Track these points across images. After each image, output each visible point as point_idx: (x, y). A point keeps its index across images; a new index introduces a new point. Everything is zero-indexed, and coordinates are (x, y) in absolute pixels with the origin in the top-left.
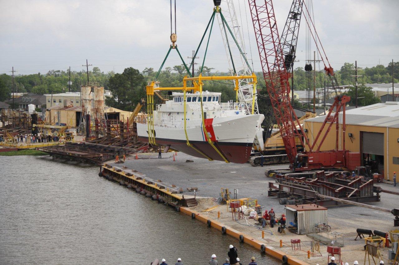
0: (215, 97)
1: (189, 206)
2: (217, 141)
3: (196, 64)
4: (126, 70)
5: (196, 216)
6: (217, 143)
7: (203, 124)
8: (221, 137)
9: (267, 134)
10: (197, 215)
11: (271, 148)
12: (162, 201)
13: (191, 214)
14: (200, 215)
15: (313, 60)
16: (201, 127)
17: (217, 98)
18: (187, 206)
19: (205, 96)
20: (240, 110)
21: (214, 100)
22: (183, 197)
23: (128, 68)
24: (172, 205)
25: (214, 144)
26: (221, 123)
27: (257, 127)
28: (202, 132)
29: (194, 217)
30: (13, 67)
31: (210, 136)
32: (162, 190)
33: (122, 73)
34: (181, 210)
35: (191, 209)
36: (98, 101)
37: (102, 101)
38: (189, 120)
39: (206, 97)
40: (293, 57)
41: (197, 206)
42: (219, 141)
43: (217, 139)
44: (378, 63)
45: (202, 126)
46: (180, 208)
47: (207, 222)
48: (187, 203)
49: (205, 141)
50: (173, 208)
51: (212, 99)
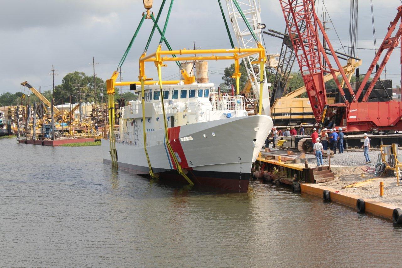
1: (317, 180)
3: (327, 29)
5: (332, 196)
6: (191, 173)
7: (166, 139)
8: (196, 162)
9: (277, 91)
10: (334, 193)
11: (281, 114)
12: (269, 178)
13: (322, 194)
14: (342, 193)
16: (164, 143)
18: (314, 182)
19: (184, 89)
20: (233, 111)
21: (200, 95)
22: (306, 165)
24: (287, 183)
25: (186, 175)
28: (167, 153)
30: (40, 87)
31: (179, 160)
34: (303, 189)
35: (321, 185)
36: (200, 79)
37: (206, 79)
38: (154, 130)
39: (186, 91)
41: (335, 181)
42: (194, 169)
45: (166, 141)
46: (300, 185)
47: (355, 204)
48: (314, 176)
49: (173, 168)
50: (289, 187)
51: (197, 94)
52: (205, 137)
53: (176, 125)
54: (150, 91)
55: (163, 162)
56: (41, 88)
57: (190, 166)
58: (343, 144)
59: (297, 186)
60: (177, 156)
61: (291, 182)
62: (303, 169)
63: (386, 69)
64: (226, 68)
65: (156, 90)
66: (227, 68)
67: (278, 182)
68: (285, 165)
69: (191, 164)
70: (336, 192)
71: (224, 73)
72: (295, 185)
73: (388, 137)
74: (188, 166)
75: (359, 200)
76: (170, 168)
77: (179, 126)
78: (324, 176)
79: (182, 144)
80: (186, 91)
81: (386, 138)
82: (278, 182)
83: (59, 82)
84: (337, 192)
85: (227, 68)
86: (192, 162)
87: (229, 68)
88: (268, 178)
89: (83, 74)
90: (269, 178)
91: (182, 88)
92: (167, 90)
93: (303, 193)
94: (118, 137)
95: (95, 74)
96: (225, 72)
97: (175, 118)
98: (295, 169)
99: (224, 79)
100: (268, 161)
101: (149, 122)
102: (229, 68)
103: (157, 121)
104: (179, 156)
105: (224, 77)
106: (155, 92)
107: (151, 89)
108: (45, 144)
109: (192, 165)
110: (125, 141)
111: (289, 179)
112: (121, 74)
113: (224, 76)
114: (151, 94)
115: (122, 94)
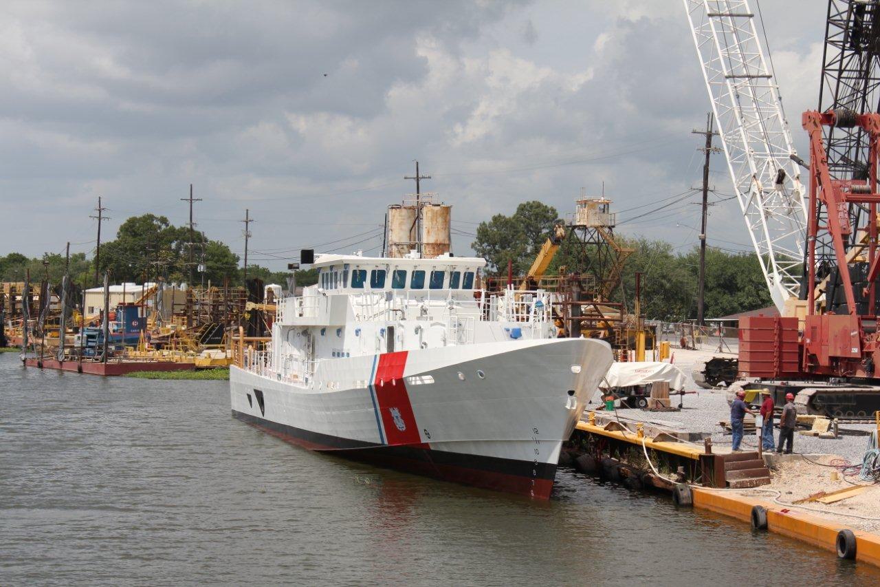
0: (458, 273)
1: (732, 481)
2: (427, 444)
4: (522, 209)
8: (439, 431)
10: (777, 514)
15: (840, 12)
17: (469, 276)
18: (727, 485)
19: (418, 269)
22: (708, 448)
23: (528, 203)
26: (432, 373)
27: (571, 393)
29: (759, 523)
30: (69, 244)
32: (617, 434)
33: (512, 216)
34: (697, 503)
39: (423, 273)
40: (848, 45)
43: (424, 440)
44: (744, 441)
46: (691, 490)
51: (446, 281)
52: (462, 378)
53: (398, 348)
54: (346, 268)
55: (365, 429)
56: (70, 246)
57: (424, 440)
58: (135, 362)
59: (684, 494)
60: (397, 417)
61: (670, 484)
62: (700, 456)
63: (193, 198)
64: (482, 223)
65: (358, 266)
66: (484, 224)
67: (636, 481)
68: (655, 446)
69: (426, 437)
70: (783, 511)
71: (476, 233)
72: (682, 490)
73: (861, 394)
74: (419, 440)
75: (842, 532)
76: (379, 442)
77: (404, 350)
78: (748, 475)
79: (409, 391)
80: (423, 273)
81: (867, 394)
82: (636, 481)
83: (110, 235)
84: (786, 511)
85: (484, 224)
86: (428, 431)
87: (487, 223)
88: (612, 471)
89: (164, 220)
90: (614, 472)
91: (415, 266)
92: (383, 268)
93: (697, 508)
94: (268, 364)
95: (193, 221)
96: (479, 232)
97: (397, 332)
98: (680, 454)
99: (476, 249)
100: (613, 435)
101: (338, 335)
102: (487, 223)
103: (357, 335)
104: (402, 417)
105: (476, 243)
106: (355, 272)
107: (346, 265)
108: (84, 371)
109: (429, 438)
110: (283, 375)
111: (665, 477)
112: (248, 224)
113: (477, 240)
114: (346, 274)
115: (70, 256)
